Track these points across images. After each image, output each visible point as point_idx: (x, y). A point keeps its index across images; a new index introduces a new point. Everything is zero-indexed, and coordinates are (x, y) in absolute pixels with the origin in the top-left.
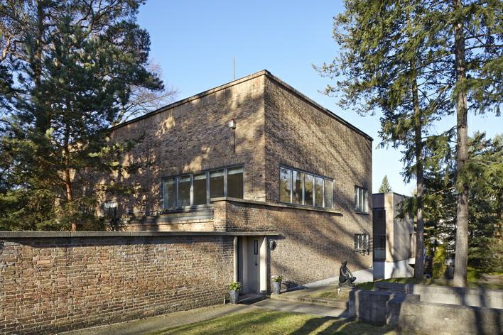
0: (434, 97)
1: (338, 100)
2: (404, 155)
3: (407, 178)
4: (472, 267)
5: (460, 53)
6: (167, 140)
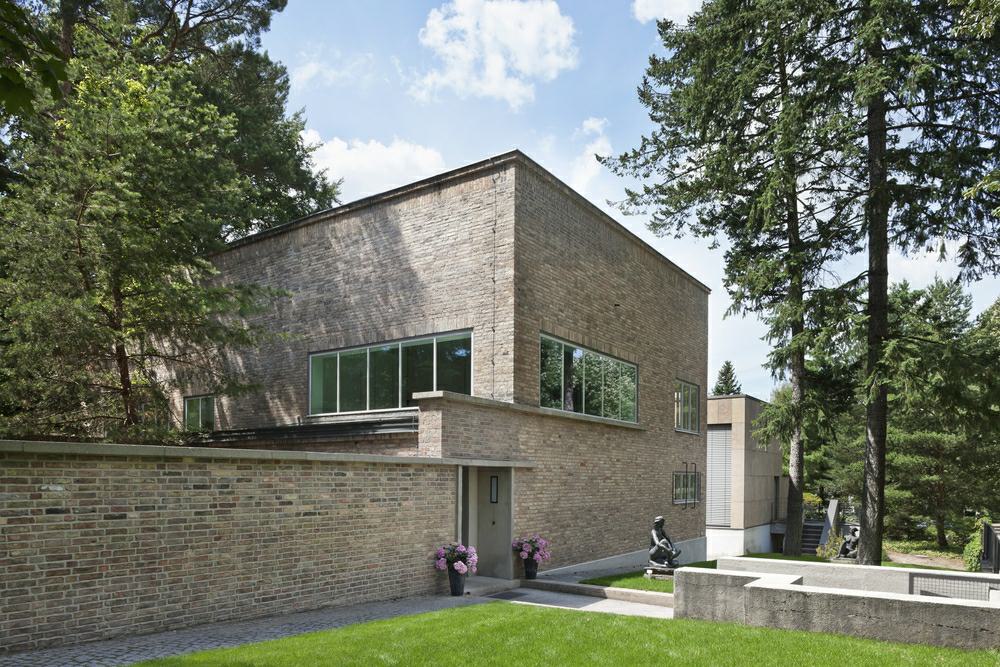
0: (826, 216)
1: (649, 219)
2: (768, 328)
3: (778, 371)
4: (875, 441)
5: (878, 163)
6: (320, 280)
